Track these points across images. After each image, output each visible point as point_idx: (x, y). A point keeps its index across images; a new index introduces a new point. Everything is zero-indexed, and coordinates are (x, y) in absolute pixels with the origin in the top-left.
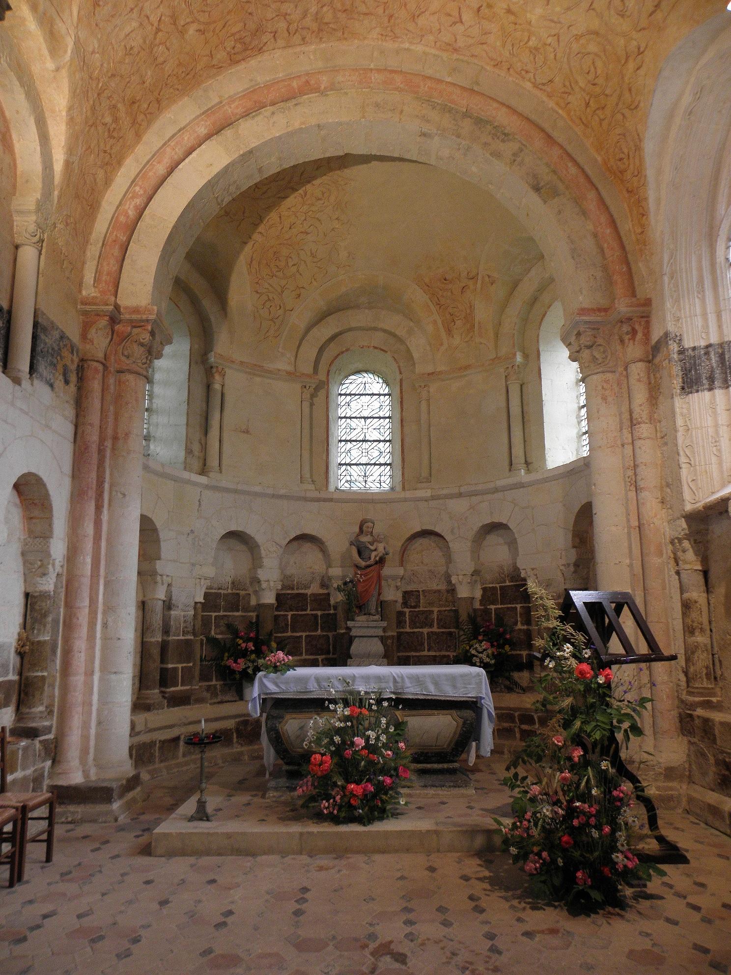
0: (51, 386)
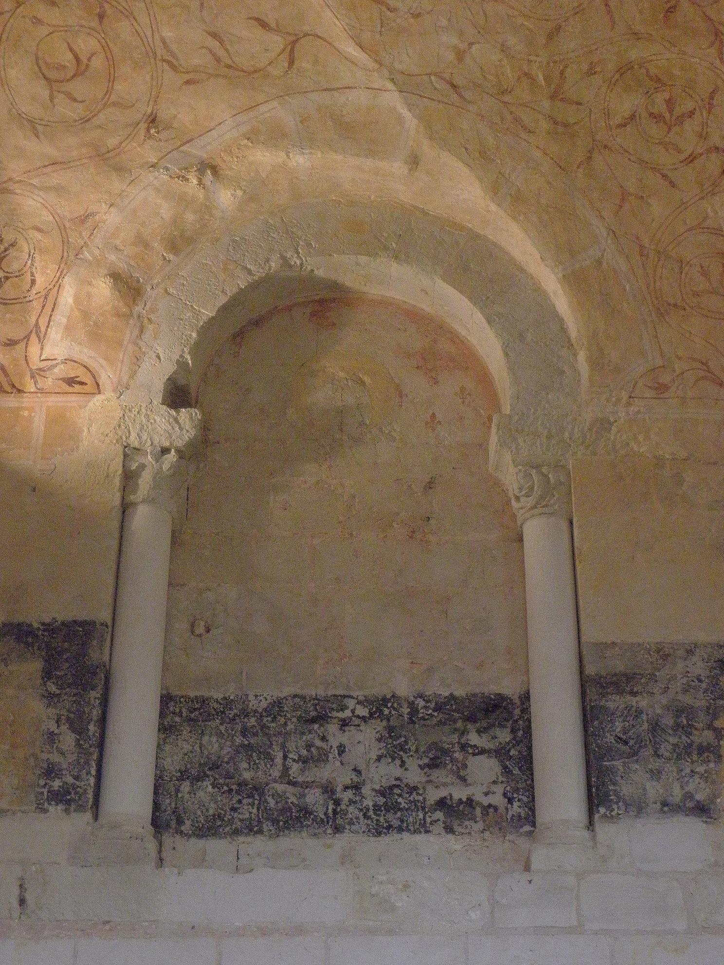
0: (702, 810)
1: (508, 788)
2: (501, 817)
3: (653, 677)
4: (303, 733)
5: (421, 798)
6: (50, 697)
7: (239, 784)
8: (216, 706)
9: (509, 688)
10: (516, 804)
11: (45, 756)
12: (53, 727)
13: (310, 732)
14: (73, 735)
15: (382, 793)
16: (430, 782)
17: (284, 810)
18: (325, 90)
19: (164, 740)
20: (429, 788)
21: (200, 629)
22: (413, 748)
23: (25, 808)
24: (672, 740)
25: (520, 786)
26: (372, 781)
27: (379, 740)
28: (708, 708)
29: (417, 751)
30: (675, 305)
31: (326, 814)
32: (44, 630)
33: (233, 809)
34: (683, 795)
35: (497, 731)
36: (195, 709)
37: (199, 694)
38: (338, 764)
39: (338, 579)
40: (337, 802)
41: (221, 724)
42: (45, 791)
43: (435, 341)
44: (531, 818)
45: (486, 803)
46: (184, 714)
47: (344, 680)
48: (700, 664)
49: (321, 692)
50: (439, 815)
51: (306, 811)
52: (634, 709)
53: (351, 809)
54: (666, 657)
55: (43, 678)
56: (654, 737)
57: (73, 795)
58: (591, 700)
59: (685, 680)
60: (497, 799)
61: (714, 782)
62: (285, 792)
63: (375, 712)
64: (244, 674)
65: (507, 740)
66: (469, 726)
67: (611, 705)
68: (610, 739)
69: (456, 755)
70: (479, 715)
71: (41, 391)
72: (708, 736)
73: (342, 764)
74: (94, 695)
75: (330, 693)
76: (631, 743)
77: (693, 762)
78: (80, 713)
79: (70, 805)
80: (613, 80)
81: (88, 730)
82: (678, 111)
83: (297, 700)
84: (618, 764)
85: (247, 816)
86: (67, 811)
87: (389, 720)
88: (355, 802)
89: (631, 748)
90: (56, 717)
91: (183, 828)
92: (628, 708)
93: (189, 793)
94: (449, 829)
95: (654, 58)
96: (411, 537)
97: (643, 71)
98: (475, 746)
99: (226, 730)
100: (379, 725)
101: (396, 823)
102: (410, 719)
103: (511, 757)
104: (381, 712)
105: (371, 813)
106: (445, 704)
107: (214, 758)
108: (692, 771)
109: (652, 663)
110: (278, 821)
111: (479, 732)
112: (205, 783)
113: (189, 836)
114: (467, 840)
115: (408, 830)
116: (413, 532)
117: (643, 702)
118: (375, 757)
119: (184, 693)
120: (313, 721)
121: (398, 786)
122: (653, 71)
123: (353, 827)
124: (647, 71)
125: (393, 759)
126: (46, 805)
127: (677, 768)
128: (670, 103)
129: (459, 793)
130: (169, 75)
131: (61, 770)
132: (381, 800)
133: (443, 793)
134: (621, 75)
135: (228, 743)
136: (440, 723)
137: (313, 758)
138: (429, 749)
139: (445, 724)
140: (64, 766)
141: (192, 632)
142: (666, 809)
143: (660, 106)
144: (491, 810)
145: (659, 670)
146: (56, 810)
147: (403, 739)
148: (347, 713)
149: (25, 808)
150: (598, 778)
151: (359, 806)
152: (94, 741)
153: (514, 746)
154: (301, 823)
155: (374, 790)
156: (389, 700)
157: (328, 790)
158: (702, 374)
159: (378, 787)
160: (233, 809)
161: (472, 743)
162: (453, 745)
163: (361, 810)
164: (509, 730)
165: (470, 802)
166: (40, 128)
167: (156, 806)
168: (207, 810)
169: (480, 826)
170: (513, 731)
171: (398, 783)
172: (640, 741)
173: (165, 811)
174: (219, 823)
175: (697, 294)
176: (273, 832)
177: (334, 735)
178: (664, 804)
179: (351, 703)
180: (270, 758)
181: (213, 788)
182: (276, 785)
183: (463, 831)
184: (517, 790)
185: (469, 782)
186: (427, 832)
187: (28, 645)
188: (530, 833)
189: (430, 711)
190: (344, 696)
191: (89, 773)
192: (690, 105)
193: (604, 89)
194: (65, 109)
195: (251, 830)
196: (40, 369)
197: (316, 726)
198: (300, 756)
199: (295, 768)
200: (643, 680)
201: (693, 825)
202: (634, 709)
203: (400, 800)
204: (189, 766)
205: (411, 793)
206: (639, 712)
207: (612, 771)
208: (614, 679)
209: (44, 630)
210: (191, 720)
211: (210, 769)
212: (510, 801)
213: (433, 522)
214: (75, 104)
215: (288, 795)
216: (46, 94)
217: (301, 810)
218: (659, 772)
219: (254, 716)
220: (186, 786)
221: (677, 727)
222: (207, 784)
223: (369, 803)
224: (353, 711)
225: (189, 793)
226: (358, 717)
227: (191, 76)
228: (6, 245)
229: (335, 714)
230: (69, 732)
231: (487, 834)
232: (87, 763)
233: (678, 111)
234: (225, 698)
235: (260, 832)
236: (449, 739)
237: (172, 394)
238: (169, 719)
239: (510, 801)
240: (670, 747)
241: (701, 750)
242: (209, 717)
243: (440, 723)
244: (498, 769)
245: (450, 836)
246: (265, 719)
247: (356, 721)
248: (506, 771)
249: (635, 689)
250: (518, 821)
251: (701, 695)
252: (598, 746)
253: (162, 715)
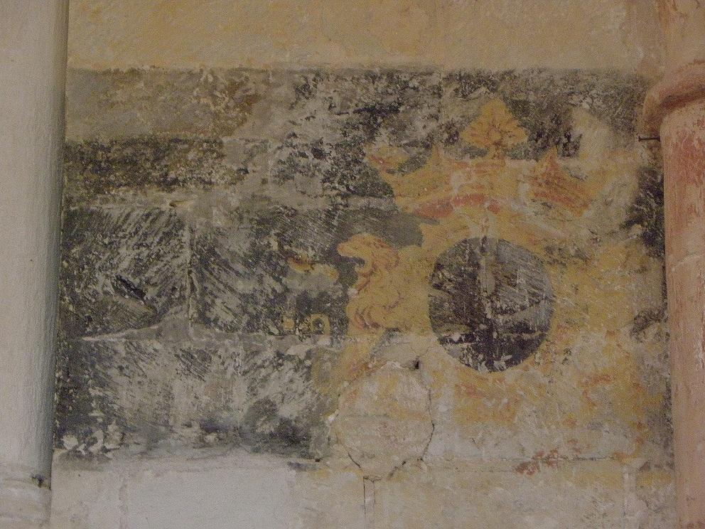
0: (291, 440)
67: (114, 210)
117: (187, 203)
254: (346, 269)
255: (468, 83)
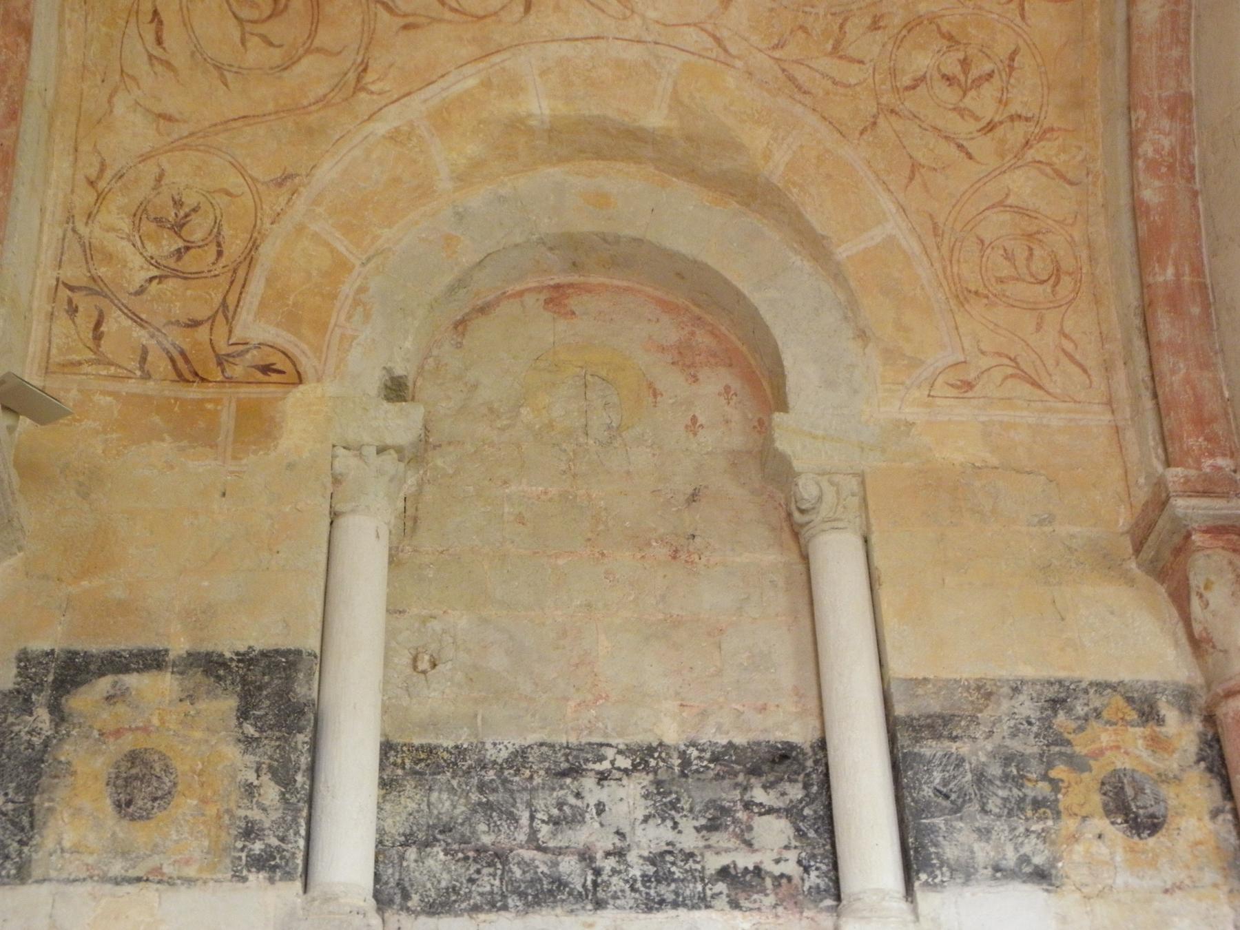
0: (1042, 876)
1: (803, 855)
2: (796, 887)
3: (974, 719)
4: (553, 789)
5: (698, 867)
6: (248, 742)
7: (477, 851)
8: (446, 755)
9: (799, 734)
10: (813, 874)
11: (242, 813)
12: (251, 777)
13: (561, 788)
14: (277, 788)
15: (652, 861)
16: (708, 847)
17: (532, 882)
18: (567, 40)
19: (384, 797)
20: (708, 854)
21: (424, 664)
22: (687, 807)
23: (220, 876)
24: (1001, 793)
25: (816, 851)
26: (638, 846)
27: (646, 797)
28: (1041, 756)
29: (691, 810)
30: (976, 293)
31: (584, 886)
32: (239, 661)
33: (471, 881)
34: (1019, 859)
35: (787, 786)
36: (421, 760)
37: (424, 741)
38: (597, 825)
39: (589, 605)
40: (597, 872)
41: (453, 777)
42: (243, 855)
43: (693, 334)
44: (835, 891)
45: (777, 873)
46: (408, 766)
47: (600, 725)
48: (1028, 703)
49: (573, 740)
50: (721, 887)
51: (560, 883)
52: (954, 757)
53: (615, 880)
54: (988, 695)
55: (238, 719)
56: (980, 789)
57: (278, 860)
58: (902, 747)
59: (1012, 723)
60: (791, 868)
61: (1053, 843)
62: (533, 860)
63: (640, 764)
64: (479, 717)
65: (799, 797)
66: (753, 780)
67: (927, 752)
68: (927, 792)
69: (739, 815)
70: (765, 768)
71: (230, 380)
72: (1044, 788)
73: (602, 825)
74: (302, 738)
75: (584, 741)
76: (953, 796)
77: (1027, 819)
78: (285, 761)
79: (274, 872)
80: (900, 37)
81: (295, 781)
82: (975, 73)
83: (544, 749)
84: (939, 821)
85: (488, 888)
86: (271, 880)
87: (656, 773)
88: (620, 872)
89: (953, 802)
90: (255, 765)
91: (410, 904)
92: (947, 755)
93: (416, 861)
94: (735, 905)
95: (947, 12)
96: (674, 558)
97: (934, 27)
98: (761, 804)
99: (460, 785)
100: (646, 779)
101: (670, 897)
102: (682, 772)
103: (805, 817)
104: (647, 763)
105: (639, 885)
106: (724, 754)
107: (445, 818)
108: (1027, 830)
109: (972, 702)
110: (526, 895)
111: (765, 787)
112: (435, 849)
113: (417, 914)
114: (756, 917)
115: (685, 905)
116: (676, 551)
118: (641, 818)
119: (407, 741)
120: (564, 774)
121: (670, 853)
122: (945, 28)
123: (618, 902)
124: (939, 27)
125: (664, 820)
126: (245, 873)
127: (1009, 826)
128: (965, 63)
129: (745, 860)
130: (384, 15)
131: (263, 830)
132: (651, 870)
133: (724, 860)
134: (909, 31)
135: (462, 801)
136: (718, 777)
137: (565, 819)
138: (707, 808)
139: (723, 778)
140: (267, 825)
141: (415, 668)
142: (999, 875)
143: (953, 68)
144: (784, 881)
145: (981, 711)
146: (256, 879)
147: (674, 796)
148: (606, 765)
149: (220, 876)
150: (916, 839)
151: (623, 876)
152: (303, 794)
153: (807, 805)
154: (555, 897)
155: (641, 856)
156: (655, 749)
157: (586, 856)
158: (1010, 371)
159: (646, 854)
160: (471, 881)
161: (758, 801)
162: (735, 802)
163: (627, 881)
164: (800, 785)
165: (758, 871)
166: (229, 76)
167: (377, 878)
168: (439, 882)
169: (770, 900)
170: (806, 786)
171: (670, 848)
172: (962, 792)
173: (386, 883)
174: (454, 898)
175: (1001, 281)
176: (521, 908)
177: (591, 791)
178: (997, 869)
179: (610, 753)
180: (513, 818)
181: (446, 854)
182: (522, 852)
183: (751, 906)
184: (814, 856)
185: (756, 846)
186: (708, 907)
187: (219, 678)
188: (831, 909)
189: (705, 763)
190: (601, 745)
191: (297, 833)
192: (988, 67)
193: (889, 47)
194: (256, 53)
195: (494, 906)
196: (228, 355)
197: (568, 781)
198: (550, 816)
199: (544, 831)
200: (963, 723)
201: (1032, 894)
202: (954, 757)
203: (673, 869)
204: (415, 828)
205: (686, 861)
206: (960, 761)
207: (932, 829)
208: (929, 721)
209: (239, 661)
210: (416, 773)
211: (442, 832)
212: (807, 870)
213: (698, 540)
214: (271, 49)
215: (537, 863)
216: (236, 35)
217: (553, 882)
218: (988, 831)
219: (493, 768)
220: (412, 853)
221: (1006, 778)
222: (438, 850)
223: (636, 872)
224: (612, 762)
225: (416, 861)
226: (619, 769)
227: (410, 20)
228: (187, 210)
229: (591, 766)
230: (272, 784)
231: (780, 910)
232: (295, 820)
233: (975, 73)
234: (456, 747)
235: (505, 908)
236: (730, 796)
237: (386, 387)
238: (388, 771)
239: (807, 870)
240: (999, 802)
241: (1037, 804)
242: (438, 770)
243: (718, 777)
244: (791, 832)
245: (737, 913)
246: (506, 772)
247: (617, 774)
248: (800, 834)
249: (954, 734)
250: (816, 894)
251: (1032, 740)
252: (913, 800)
253: (382, 768)
254: (1055, 784)
255: (1101, 686)
